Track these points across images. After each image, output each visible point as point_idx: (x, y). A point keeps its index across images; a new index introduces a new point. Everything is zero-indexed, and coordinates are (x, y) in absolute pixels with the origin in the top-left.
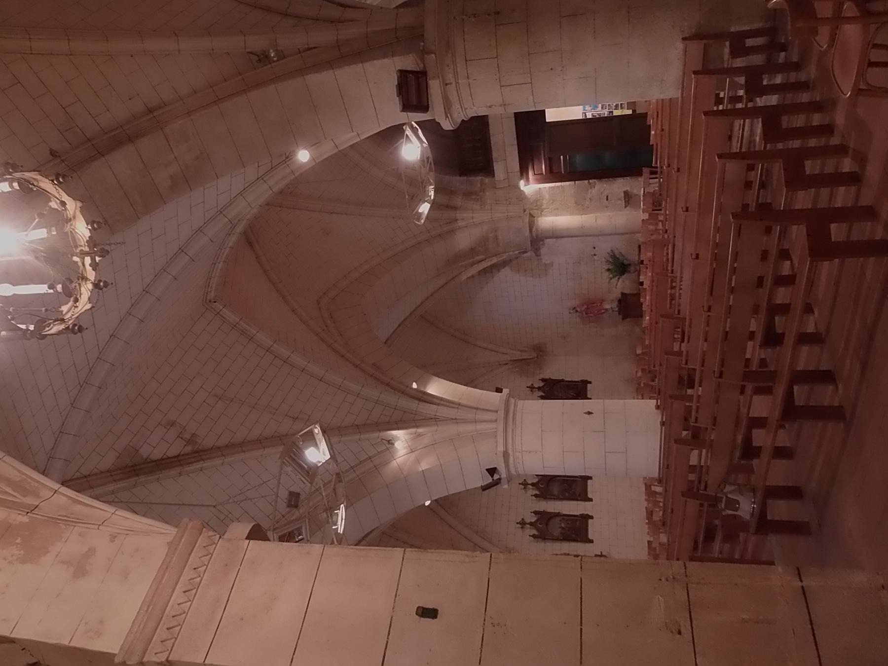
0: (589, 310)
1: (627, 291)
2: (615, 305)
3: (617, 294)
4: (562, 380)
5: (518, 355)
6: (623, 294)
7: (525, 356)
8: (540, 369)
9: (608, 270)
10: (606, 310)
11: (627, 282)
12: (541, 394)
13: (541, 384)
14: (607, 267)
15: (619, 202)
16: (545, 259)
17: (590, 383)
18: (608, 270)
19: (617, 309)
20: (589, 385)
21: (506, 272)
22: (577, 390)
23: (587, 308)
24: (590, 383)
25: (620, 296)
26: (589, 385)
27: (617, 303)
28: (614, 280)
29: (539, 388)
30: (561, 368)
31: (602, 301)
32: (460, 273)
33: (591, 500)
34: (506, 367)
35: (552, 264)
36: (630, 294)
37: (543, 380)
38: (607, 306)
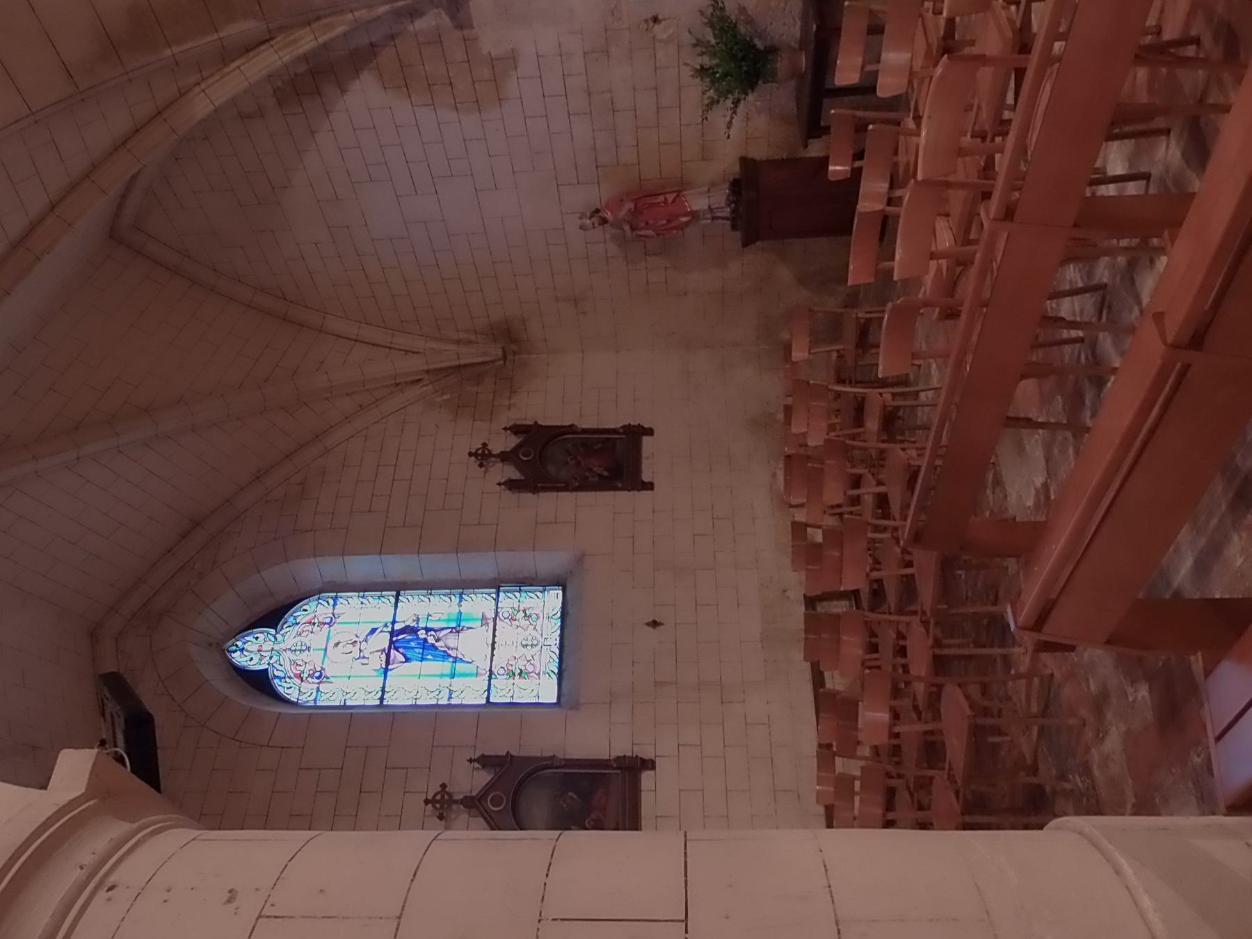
0: (643, 216)
1: (759, 152)
2: (720, 198)
3: (726, 162)
4: (571, 429)
5: (448, 355)
6: (745, 162)
7: (469, 355)
8: (513, 392)
9: (703, 71)
10: (694, 215)
11: (761, 122)
12: (512, 473)
13: (512, 441)
14: (697, 62)
15: (445, 693)
16: (490, 41)
17: (650, 432)
18: (703, 71)
19: (727, 212)
20: (646, 440)
21: (364, 96)
22: (610, 460)
23: (636, 212)
24: (650, 432)
25: (737, 168)
26: (646, 440)
27: (725, 190)
28: (719, 116)
29: (504, 457)
30: (571, 391)
31: (682, 186)
32: (182, 94)
33: (649, 486)
34: (413, 392)
35: (512, 58)
36: (770, 163)
37: (516, 430)
38: (698, 203)
